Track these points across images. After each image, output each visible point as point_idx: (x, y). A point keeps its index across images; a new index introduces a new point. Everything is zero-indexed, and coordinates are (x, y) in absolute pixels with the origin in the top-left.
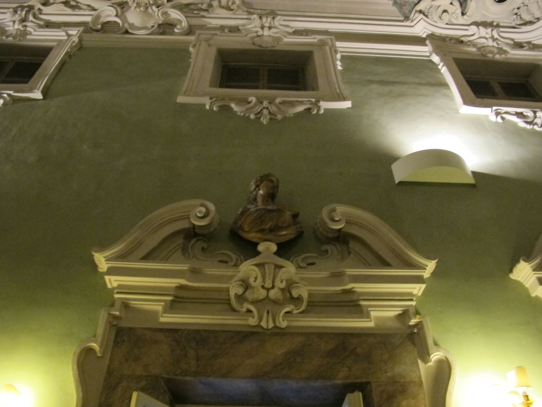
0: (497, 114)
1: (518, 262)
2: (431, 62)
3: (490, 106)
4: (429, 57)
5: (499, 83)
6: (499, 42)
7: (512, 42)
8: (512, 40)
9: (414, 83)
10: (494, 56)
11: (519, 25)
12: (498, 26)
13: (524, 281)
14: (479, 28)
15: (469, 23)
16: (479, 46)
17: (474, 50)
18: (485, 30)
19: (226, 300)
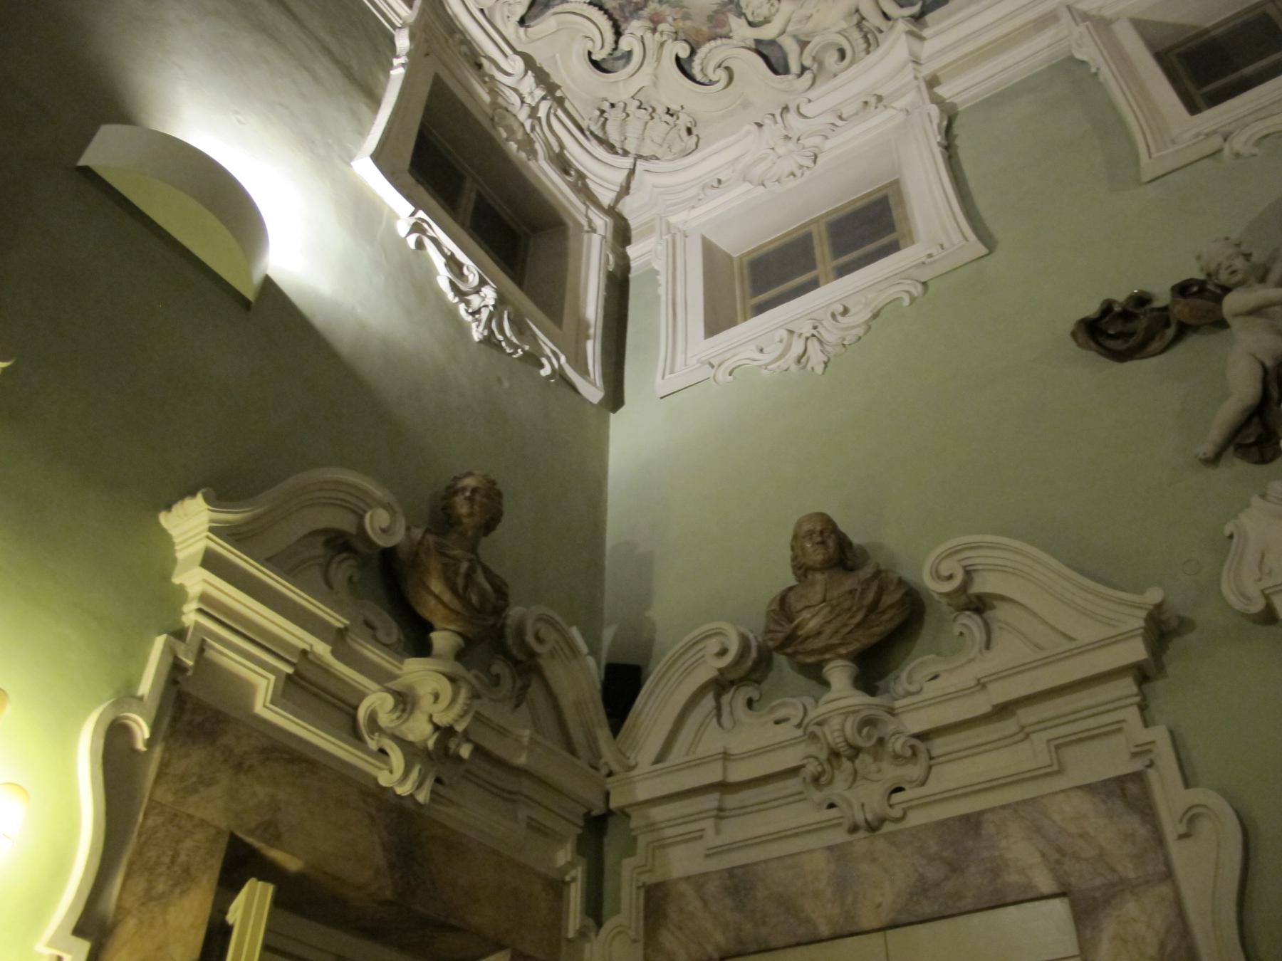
0: (417, 228)
1: (192, 494)
2: (391, 40)
3: (418, 205)
4: (394, 27)
5: (479, 195)
6: (538, 129)
7: (557, 149)
8: (562, 146)
9: (318, 40)
10: (507, 140)
11: (592, 133)
12: (560, 102)
13: (182, 543)
14: (526, 73)
15: (519, 49)
16: (500, 100)
17: (487, 98)
18: (534, 86)
19: (349, 705)
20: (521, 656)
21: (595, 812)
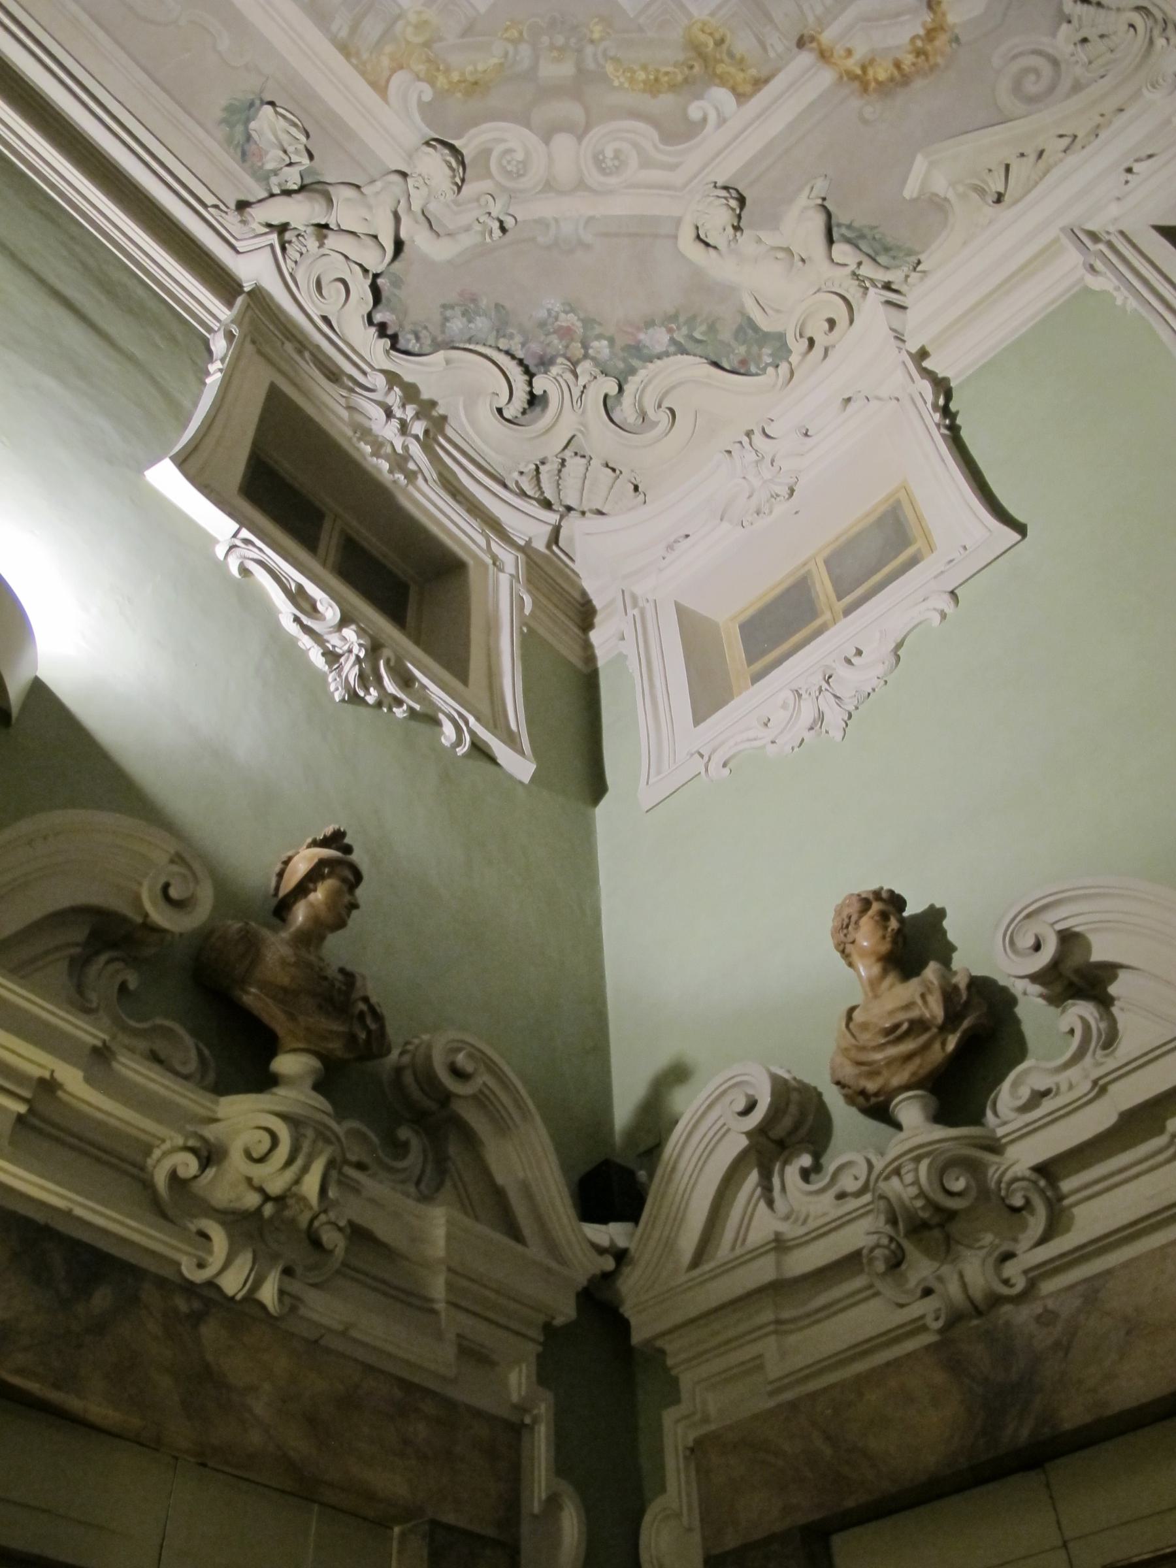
3: (243, 521)
20: (428, 1104)
21: (559, 1321)
